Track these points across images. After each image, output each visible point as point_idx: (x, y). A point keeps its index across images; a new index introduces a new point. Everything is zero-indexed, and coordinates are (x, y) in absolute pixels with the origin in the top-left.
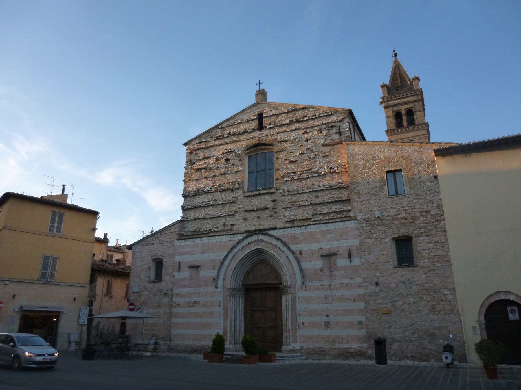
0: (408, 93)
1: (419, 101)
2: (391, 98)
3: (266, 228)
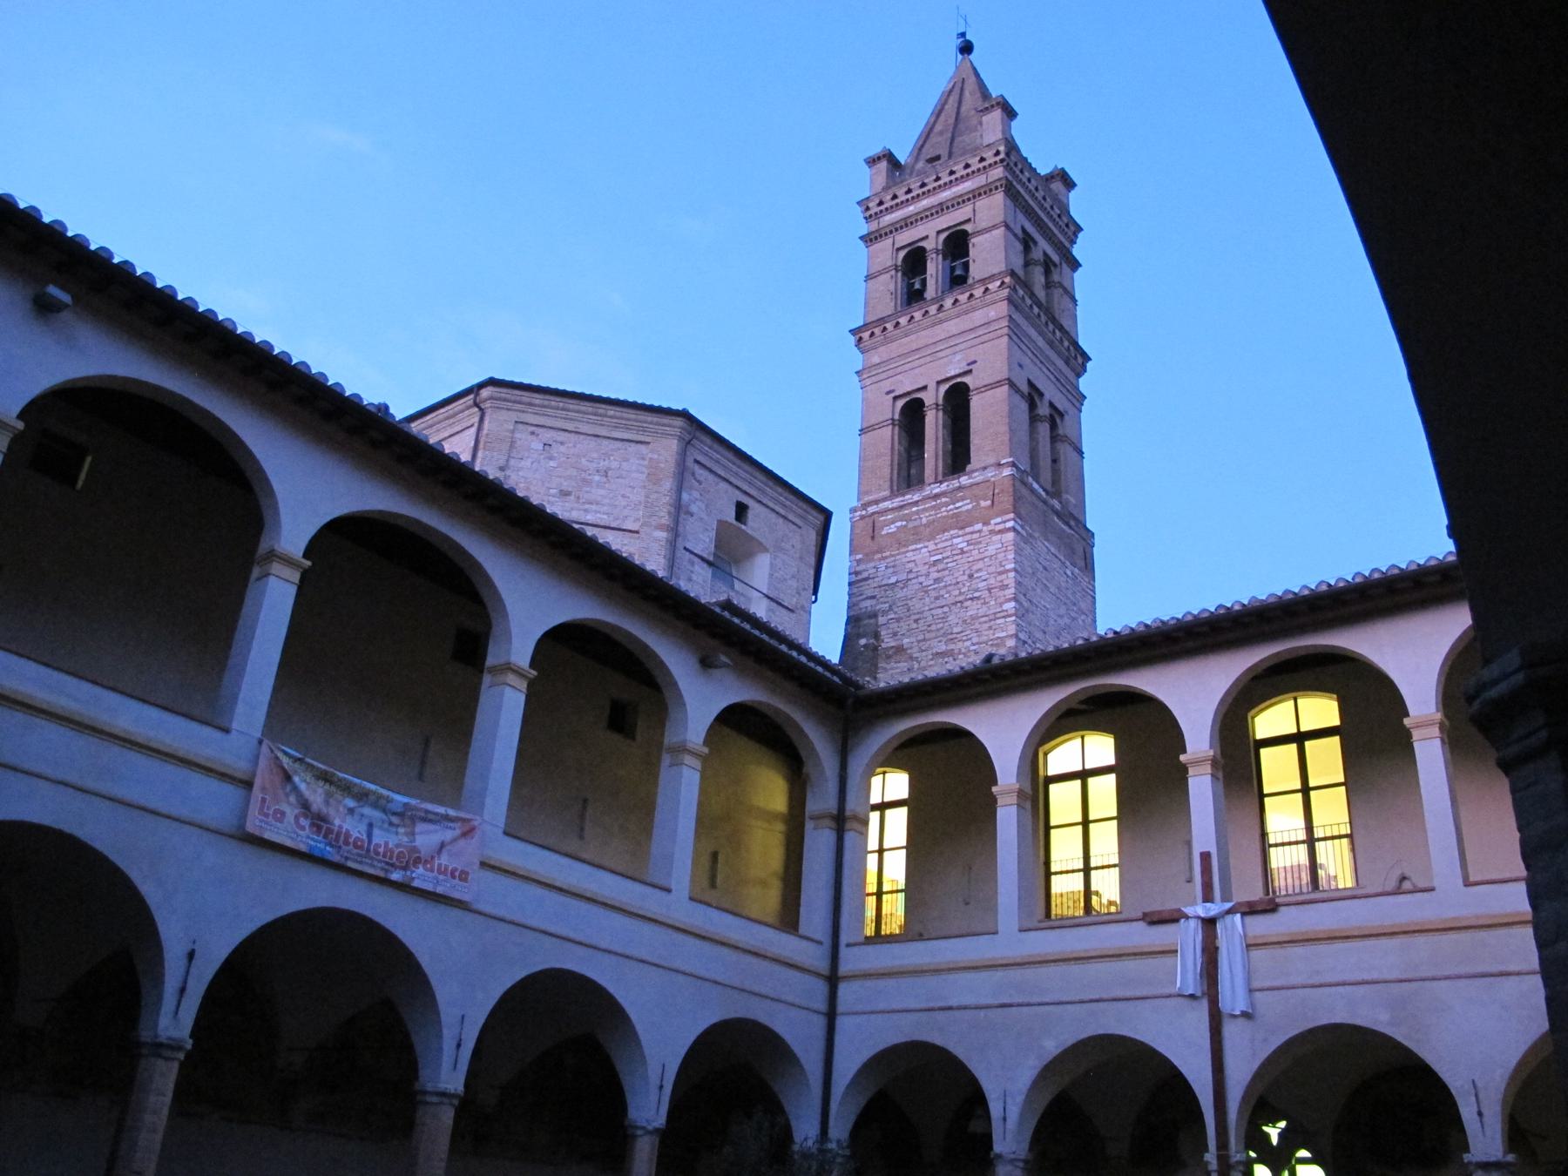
0: (954, 169)
3: (746, 739)
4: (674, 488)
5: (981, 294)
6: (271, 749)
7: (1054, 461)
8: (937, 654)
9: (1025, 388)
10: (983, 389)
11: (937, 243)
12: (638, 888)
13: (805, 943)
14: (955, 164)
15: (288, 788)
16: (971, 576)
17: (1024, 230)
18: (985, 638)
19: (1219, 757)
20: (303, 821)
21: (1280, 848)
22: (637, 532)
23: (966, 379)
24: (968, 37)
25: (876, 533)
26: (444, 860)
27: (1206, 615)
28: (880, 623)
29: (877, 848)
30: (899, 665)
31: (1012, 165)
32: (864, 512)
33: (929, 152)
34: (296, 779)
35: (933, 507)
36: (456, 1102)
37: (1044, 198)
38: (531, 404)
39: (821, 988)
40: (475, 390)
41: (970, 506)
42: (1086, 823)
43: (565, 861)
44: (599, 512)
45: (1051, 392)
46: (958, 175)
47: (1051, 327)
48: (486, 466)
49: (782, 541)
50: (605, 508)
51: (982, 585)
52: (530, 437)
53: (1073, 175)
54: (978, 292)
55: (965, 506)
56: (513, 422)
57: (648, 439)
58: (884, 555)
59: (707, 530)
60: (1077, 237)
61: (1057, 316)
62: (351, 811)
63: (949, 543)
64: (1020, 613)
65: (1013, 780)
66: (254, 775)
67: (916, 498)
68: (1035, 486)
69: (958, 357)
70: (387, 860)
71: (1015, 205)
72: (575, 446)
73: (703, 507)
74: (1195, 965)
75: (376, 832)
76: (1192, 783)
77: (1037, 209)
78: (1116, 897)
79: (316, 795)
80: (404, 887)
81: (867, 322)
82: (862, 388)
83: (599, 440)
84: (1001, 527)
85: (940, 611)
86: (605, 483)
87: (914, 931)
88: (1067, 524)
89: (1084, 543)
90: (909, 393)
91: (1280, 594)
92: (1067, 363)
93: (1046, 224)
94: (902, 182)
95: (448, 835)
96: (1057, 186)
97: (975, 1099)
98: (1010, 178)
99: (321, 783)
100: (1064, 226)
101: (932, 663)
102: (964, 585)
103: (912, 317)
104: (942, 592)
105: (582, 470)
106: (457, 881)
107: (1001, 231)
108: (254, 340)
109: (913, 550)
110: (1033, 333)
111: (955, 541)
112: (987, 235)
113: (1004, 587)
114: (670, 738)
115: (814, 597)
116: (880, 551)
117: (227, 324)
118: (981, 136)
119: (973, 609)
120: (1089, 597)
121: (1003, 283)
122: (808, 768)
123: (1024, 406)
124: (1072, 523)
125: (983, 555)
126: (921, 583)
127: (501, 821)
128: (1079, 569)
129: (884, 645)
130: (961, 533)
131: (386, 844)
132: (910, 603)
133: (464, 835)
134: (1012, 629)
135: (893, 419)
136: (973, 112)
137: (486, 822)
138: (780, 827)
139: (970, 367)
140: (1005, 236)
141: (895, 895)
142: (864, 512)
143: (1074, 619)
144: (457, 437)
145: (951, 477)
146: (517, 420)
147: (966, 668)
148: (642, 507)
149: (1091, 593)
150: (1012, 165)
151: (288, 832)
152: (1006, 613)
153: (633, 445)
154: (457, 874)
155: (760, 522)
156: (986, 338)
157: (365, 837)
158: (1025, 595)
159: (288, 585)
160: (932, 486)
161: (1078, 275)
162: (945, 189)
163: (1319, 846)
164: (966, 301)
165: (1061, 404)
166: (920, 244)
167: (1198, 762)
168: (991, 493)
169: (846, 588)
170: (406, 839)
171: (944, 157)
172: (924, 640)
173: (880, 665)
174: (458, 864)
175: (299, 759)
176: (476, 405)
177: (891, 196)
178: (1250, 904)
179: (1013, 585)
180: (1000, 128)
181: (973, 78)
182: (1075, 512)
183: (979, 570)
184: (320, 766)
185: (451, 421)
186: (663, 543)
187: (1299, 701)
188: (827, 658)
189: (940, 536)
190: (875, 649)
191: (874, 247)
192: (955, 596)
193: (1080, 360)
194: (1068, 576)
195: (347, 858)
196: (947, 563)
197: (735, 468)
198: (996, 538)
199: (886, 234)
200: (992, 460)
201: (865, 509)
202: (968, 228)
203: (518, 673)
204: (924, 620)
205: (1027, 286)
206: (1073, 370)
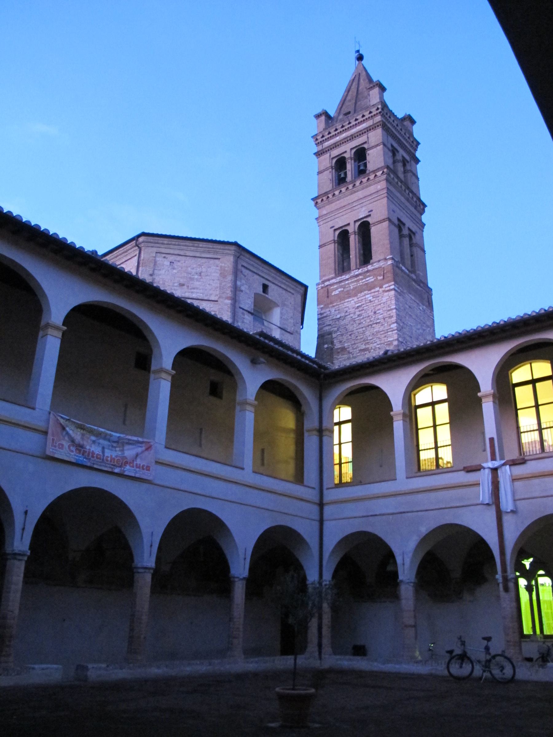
0: (357, 118)
1: (375, 127)
2: (329, 133)
4: (233, 279)
5: (373, 178)
6: (53, 414)
7: (412, 256)
8: (361, 350)
9: (396, 222)
10: (376, 224)
11: (351, 154)
12: (229, 468)
13: (307, 489)
14: (358, 115)
15: (64, 433)
16: (375, 313)
17: (392, 146)
18: (382, 342)
19: (496, 392)
20: (72, 448)
21: (526, 434)
22: (217, 301)
23: (369, 219)
24: (361, 52)
25: (329, 294)
26: (138, 461)
27: (487, 327)
28: (333, 337)
29: (338, 443)
30: (343, 356)
31: (385, 114)
32: (323, 285)
33: (345, 110)
34: (67, 429)
35: (356, 281)
36: (152, 571)
37: (401, 130)
38: (163, 244)
39: (316, 509)
40: (136, 238)
41: (373, 280)
42: (435, 426)
43: (193, 458)
44: (198, 293)
45: (409, 223)
46: (359, 121)
47: (407, 191)
48: (144, 275)
49: (285, 301)
50: (201, 290)
51: (380, 317)
52: (163, 259)
53: (414, 117)
54: (372, 177)
55: (371, 279)
56: (155, 253)
57: (219, 257)
58: (333, 305)
59: (250, 298)
60: (417, 148)
61: (410, 187)
62: (94, 442)
63: (364, 297)
64: (399, 329)
65: (400, 408)
66: (48, 428)
67: (347, 277)
68: (403, 268)
69: (364, 209)
70: (112, 463)
71: (387, 134)
72: (185, 262)
73: (247, 287)
74: (489, 490)
75: (106, 450)
76: (484, 405)
77: (398, 135)
78: (450, 459)
79: (77, 435)
80: (121, 475)
81: (320, 194)
82: (319, 226)
83: (196, 259)
84: (387, 289)
85: (361, 330)
86: (200, 279)
87: (357, 480)
88: (419, 285)
89: (427, 294)
90: (341, 227)
91: (522, 315)
92: (416, 208)
93: (403, 142)
94: (333, 125)
95: (140, 450)
96: (407, 123)
97: (390, 556)
98: (384, 121)
99: (79, 430)
100: (411, 142)
101: (359, 354)
102: (372, 317)
103: (341, 191)
104: (362, 321)
105: (189, 274)
106: (145, 471)
107: (386, 224)
108: (31, 224)
109: (347, 302)
110: (398, 195)
111: (367, 296)
112: (375, 149)
113: (391, 317)
114: (239, 398)
115: (301, 327)
116: (331, 303)
117: (18, 217)
118: (370, 101)
119: (377, 328)
120: (431, 319)
121: (383, 172)
122: (304, 408)
123: (396, 230)
124: (422, 285)
125: (380, 303)
126: (352, 317)
127: (163, 443)
128: (426, 307)
129: (336, 347)
130: (369, 292)
131: (111, 456)
132: (347, 327)
133: (147, 449)
134: (396, 337)
135: (334, 240)
136: (365, 90)
137: (157, 443)
138: (292, 435)
139: (370, 213)
140: (389, 226)
141: (347, 464)
142: (323, 285)
143: (424, 330)
144: (129, 261)
145: (363, 266)
146: (157, 251)
147: (376, 357)
148: (218, 289)
149: (432, 317)
150: (385, 114)
151: (66, 454)
152: (392, 329)
153: (212, 260)
154: (145, 467)
155: (274, 293)
156: (376, 199)
157: (101, 454)
158: (401, 320)
159: (56, 339)
160: (355, 271)
161: (419, 166)
162: (354, 128)
163: (544, 432)
164: (366, 181)
165: (414, 228)
166: (343, 155)
167: (486, 396)
168: (383, 273)
169: (317, 322)
170: (120, 453)
171: (352, 112)
172: (355, 344)
173: (335, 357)
174: (144, 463)
175: (68, 420)
176: (137, 245)
177: (328, 133)
178: (513, 461)
179: (395, 315)
180: (378, 97)
181: (364, 73)
182: (423, 280)
183: (379, 309)
184: (78, 422)
185: (126, 254)
186: (229, 306)
187: (533, 364)
188: (310, 355)
189: (359, 294)
190: (332, 349)
191: (321, 158)
192: (368, 322)
193: (422, 207)
194: (421, 310)
195: (94, 464)
196: (363, 307)
197: (261, 268)
198: (386, 294)
199: (326, 151)
200: (382, 257)
201: (324, 284)
202: (366, 146)
203: (166, 372)
204: (354, 335)
205: (395, 172)
206: (419, 212)
